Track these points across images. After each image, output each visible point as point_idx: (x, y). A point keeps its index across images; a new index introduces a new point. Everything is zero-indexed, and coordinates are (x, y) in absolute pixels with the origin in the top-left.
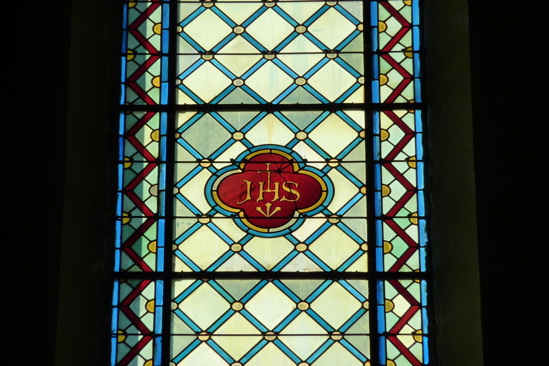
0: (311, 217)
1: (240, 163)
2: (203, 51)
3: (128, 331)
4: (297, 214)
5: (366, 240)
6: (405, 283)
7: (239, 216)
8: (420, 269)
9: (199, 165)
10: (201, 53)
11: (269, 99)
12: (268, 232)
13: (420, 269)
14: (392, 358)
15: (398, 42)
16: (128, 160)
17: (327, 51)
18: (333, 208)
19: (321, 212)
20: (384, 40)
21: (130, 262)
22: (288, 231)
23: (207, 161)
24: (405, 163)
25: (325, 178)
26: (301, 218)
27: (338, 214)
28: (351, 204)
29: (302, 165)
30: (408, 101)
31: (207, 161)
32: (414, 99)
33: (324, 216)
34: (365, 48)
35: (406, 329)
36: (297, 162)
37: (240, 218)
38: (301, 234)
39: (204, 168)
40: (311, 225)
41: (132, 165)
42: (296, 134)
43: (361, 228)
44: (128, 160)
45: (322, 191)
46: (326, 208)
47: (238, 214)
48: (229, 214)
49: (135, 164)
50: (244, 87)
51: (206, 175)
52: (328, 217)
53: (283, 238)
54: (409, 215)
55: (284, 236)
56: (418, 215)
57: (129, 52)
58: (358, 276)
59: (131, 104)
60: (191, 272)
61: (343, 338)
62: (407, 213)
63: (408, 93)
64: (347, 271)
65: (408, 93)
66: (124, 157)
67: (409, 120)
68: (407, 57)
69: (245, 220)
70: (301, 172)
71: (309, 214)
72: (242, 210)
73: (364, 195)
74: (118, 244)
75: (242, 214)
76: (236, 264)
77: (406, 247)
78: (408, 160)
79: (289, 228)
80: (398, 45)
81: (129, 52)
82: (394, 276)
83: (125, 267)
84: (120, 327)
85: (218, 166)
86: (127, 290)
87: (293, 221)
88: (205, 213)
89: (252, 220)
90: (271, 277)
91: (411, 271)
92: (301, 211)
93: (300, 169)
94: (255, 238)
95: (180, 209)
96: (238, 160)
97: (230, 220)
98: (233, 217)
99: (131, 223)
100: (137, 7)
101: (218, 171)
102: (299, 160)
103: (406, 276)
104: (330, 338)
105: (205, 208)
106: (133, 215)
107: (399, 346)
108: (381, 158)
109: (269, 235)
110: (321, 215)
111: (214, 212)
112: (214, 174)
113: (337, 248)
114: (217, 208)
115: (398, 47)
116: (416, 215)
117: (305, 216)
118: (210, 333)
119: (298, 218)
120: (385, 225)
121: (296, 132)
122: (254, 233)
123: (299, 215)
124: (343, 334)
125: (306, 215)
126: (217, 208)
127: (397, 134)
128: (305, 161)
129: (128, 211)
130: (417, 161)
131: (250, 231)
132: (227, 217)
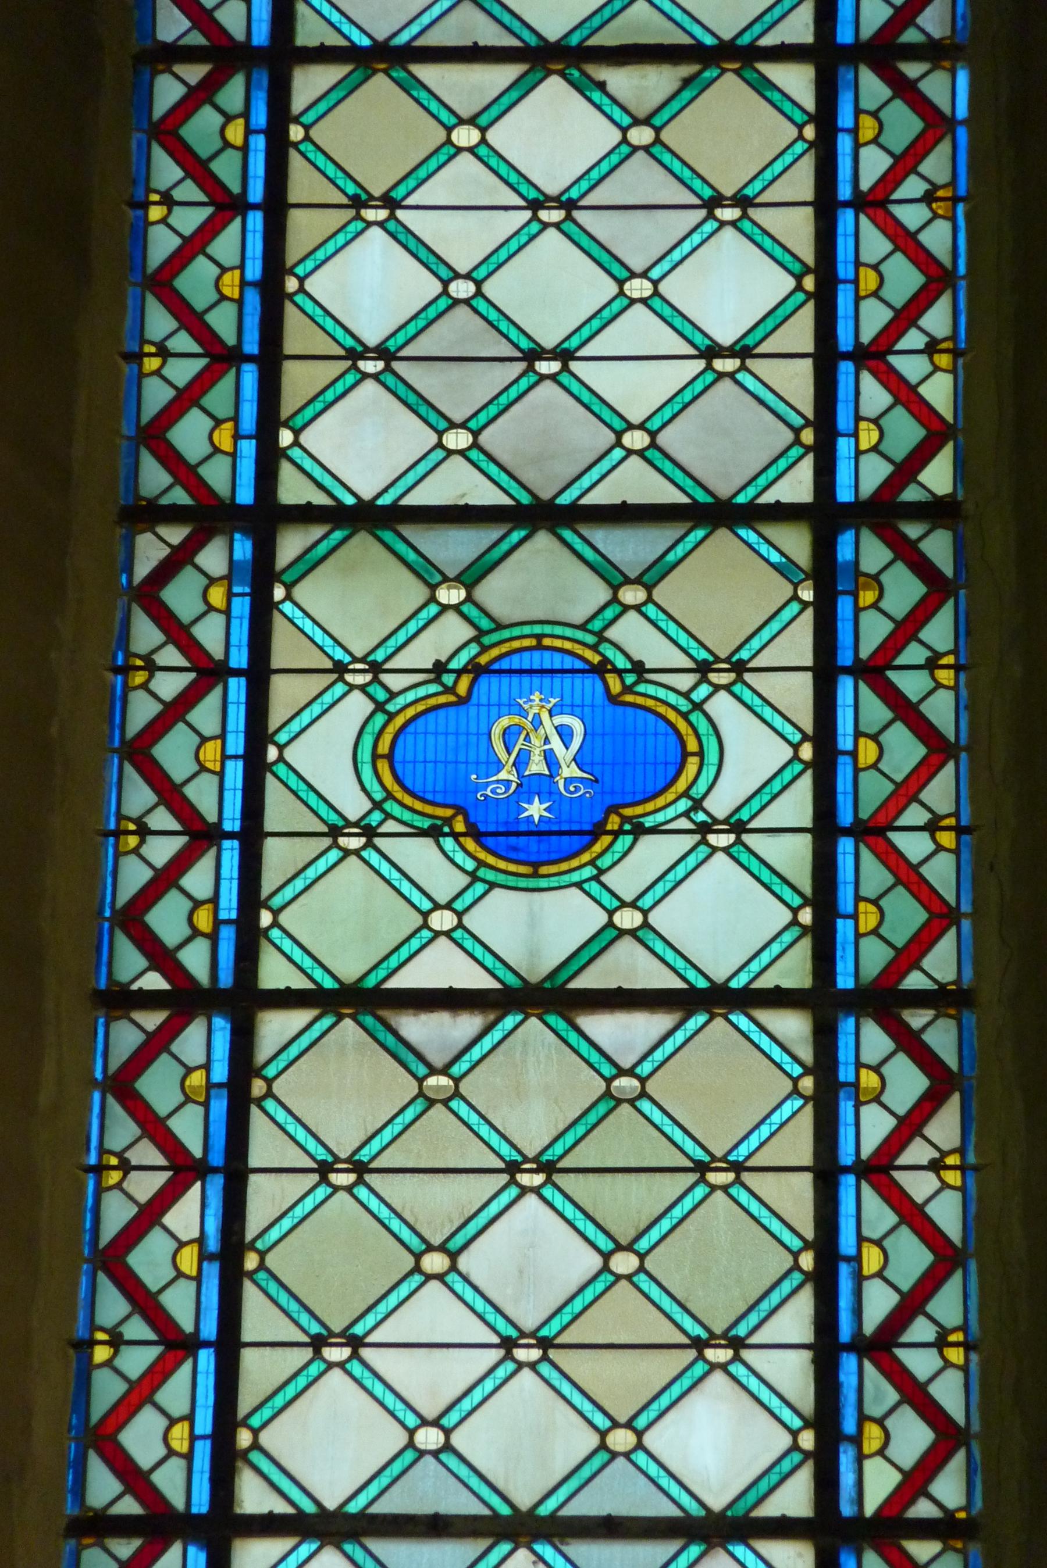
0: (655, 830)
1: (459, 673)
3: (178, 195)
6: (916, 1019)
7: (451, 828)
11: (553, 32)
13: (958, 981)
15: (914, 798)
17: (711, 352)
24: (926, 835)
25: (696, 717)
28: (769, 791)
29: (630, 679)
30: (942, 987)
32: (966, 1508)
34: (817, 1154)
37: (456, 836)
38: (627, 879)
39: (369, 224)
40: (652, 855)
42: (611, 913)
43: (797, 229)
44: (153, 350)
47: (448, 821)
48: (426, 824)
53: (575, 891)
54: (927, 192)
57: (101, 1336)
58: (782, 513)
60: (347, 47)
63: (942, 963)
64: (754, 1514)
65: (942, 963)
66: (102, 1151)
68: (936, 216)
69: (470, 844)
71: (649, 822)
72: (460, 810)
76: (441, 968)
77: (919, 751)
78: (928, 198)
81: (101, 1336)
82: (883, 1000)
89: (490, 841)
90: (535, 1005)
94: (497, 891)
96: (454, 665)
97: (428, 842)
99: (170, 221)
100: (165, 372)
107: (892, 381)
109: (537, 629)
110: (684, 824)
111: (376, 817)
112: (380, 707)
115: (913, 339)
116: (951, 821)
121: (616, 583)
123: (621, 826)
125: (642, 824)
126: (388, 806)
128: (639, 668)
130: (955, 200)
132: (421, 833)
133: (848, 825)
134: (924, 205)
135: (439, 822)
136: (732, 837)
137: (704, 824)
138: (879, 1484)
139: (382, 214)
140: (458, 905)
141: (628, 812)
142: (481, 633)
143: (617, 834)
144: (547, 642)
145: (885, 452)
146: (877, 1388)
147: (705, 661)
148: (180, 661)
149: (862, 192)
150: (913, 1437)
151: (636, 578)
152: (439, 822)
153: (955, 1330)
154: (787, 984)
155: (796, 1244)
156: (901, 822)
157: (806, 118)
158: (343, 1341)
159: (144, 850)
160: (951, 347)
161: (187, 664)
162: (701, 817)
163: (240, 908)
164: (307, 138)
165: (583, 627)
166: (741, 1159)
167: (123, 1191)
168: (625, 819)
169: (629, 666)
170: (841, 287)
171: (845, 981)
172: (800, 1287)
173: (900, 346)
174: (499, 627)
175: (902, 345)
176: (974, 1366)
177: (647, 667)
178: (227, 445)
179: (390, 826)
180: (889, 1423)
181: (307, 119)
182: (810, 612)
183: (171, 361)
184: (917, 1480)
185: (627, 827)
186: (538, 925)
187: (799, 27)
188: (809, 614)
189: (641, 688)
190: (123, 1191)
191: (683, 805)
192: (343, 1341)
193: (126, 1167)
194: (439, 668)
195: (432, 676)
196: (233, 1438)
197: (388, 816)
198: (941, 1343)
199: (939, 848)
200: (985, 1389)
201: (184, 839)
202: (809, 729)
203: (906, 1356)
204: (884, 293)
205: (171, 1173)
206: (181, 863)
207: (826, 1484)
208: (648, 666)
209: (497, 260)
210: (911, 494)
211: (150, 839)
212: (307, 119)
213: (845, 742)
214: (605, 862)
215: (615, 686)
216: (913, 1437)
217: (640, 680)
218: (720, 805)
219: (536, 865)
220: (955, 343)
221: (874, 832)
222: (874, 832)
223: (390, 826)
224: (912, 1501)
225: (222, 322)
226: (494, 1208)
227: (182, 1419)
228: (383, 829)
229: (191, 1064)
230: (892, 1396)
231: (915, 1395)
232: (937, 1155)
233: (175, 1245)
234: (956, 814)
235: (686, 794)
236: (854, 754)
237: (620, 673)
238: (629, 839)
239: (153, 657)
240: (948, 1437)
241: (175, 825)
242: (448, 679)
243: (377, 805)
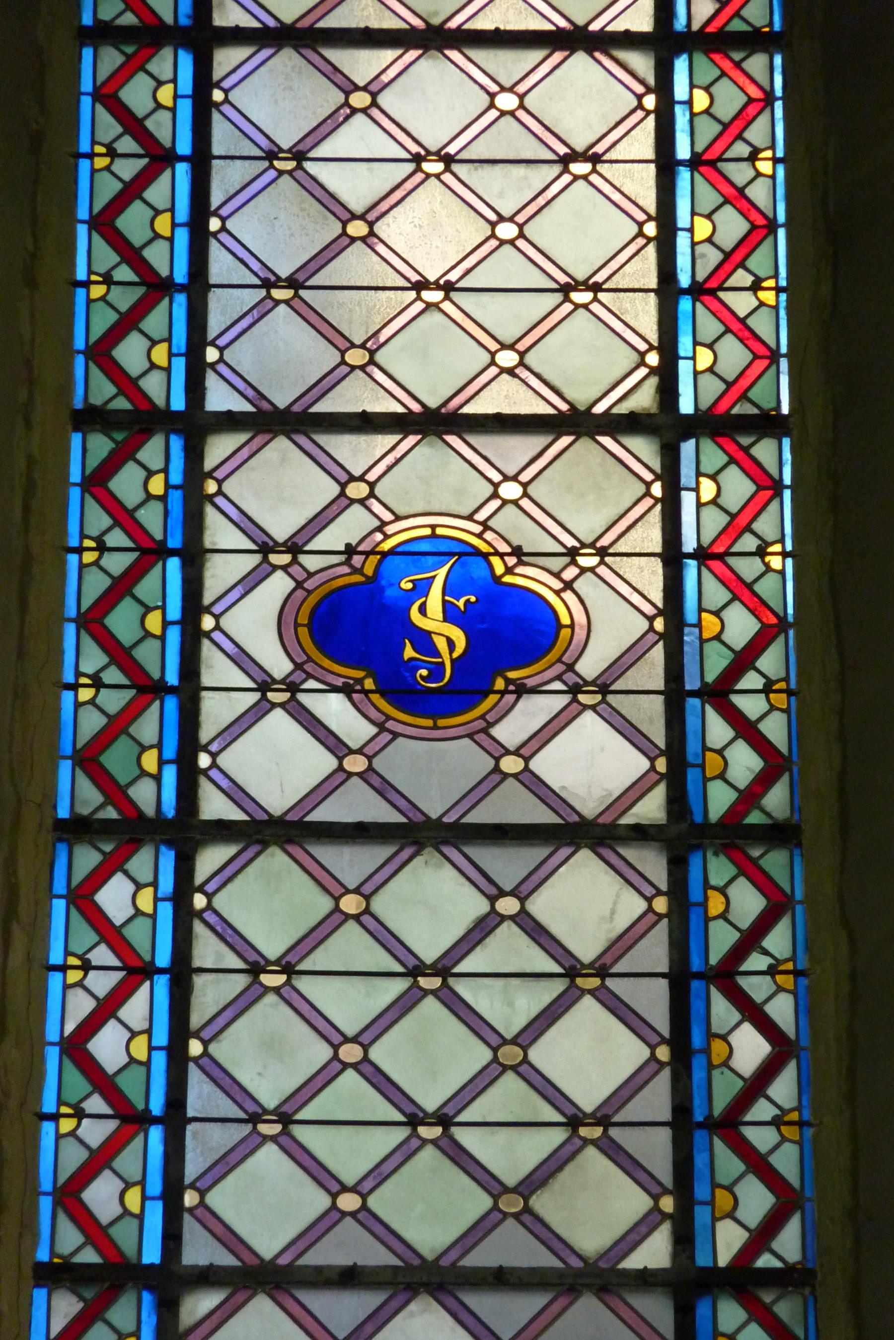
0: (535, 691)
1: (367, 554)
2: (273, 278)
4: (500, 684)
5: (656, 344)
7: (362, 685)
8: (771, 24)
9: (272, 166)
10: (267, 285)
12: (435, 727)
14: (718, 746)
16: (103, 150)
18: (589, 666)
19: (559, 678)
20: (722, 940)
21: (110, 389)
22: (481, 724)
23: (289, 155)
25: (568, 596)
26: (511, 692)
27: (598, 545)
31: (289, 155)
33: (564, 688)
35: (762, 1110)
36: (497, 553)
38: (511, 731)
41: (100, 558)
44: (103, 150)
45: (559, 626)
46: (570, 667)
47: (360, 681)
48: (339, 682)
49: (92, 974)
50: (365, 1217)
51: (278, 586)
52: (574, 690)
53: (467, 741)
54: (770, 966)
55: (470, 736)
56: (795, 965)
59: (66, 1259)
61: (602, 562)
62: (773, 1112)
65: (789, 1243)
67: (775, 862)
68: (784, 1139)
70: (508, 579)
71: (530, 683)
73: (657, 500)
74: (75, 475)
75: (369, 684)
76: (357, 805)
78: (776, 1122)
79: (483, 717)
80: (740, 272)
83: (97, 400)
84: (72, 948)
85: (311, 562)
86: (101, 446)
87: (493, 698)
88: (284, 276)
91: (750, 29)
92: (512, 675)
93: (509, 571)
94: (400, 740)
95: (217, 669)
98: (347, 690)
101: (310, 575)
102: (504, 548)
103: (770, 1277)
104: (575, 700)
105: (278, 665)
106: (116, 279)
108: (710, 1116)
110: (558, 686)
112: (299, 585)
113: (593, 763)
114: (308, 667)
115: (751, 681)
117: (521, 690)
118: (285, 1118)
119: (503, 693)
120: (710, 711)
122: (400, 728)
124: (603, 553)
125: (524, 685)
127: (748, 902)
129: (74, 1101)
131: (390, 725)
132: (334, 689)
133: (692, 551)
134: (751, 292)
135: (352, 682)
136: (599, 697)
137: (576, 685)
138: (729, 1241)
139: (276, 1129)
140: (369, 750)
141: (512, 675)
142: (485, 731)
143: (503, 693)
144: (439, 531)
145: (722, 513)
146: (729, 1245)
147: (574, 547)
148: (111, 960)
149: (698, 282)
150: (756, 1200)
151: (512, 1039)
152: (352, 682)
153: (787, 960)
154: (634, 28)
155: (649, 610)
156: (729, 283)
157: (658, 752)
158: (284, 687)
159: (103, 562)
160: (785, 687)
161: (127, 682)
162: (570, 678)
163: (184, 609)
164: (217, 627)
165: (470, 518)
166: (600, 281)
167: (102, 569)
168: (508, 681)
169: (509, 550)
170: (680, 233)
171: (686, 406)
172: (656, 643)
173: (741, 686)
174: (398, 518)
175: (742, 685)
176: (801, 989)
177: (525, 551)
178: (135, 1208)
179: (311, 684)
180: (737, 1190)
181: (217, 609)
182: (652, 117)
183: (103, 691)
184: (763, 1236)
185: (512, 688)
186: (435, 769)
187: (641, 20)
188: (651, 120)
189: (519, 570)
190: (102, 569)
191: (559, 668)
192: (284, 687)
193: (86, 967)
194: (350, 551)
195: (342, 558)
196: (198, 622)
197: (557, 575)
198: (767, 689)
199: (772, 708)
200: (814, 1158)
201: (121, 974)
202: (652, 211)
203: (750, 1133)
204: (740, 1214)
205: (125, 973)
206: (134, 574)
207: (684, 1240)
208: (526, 550)
209: (380, 1174)
210: (754, 818)
211: (85, 1121)
212: (217, 609)
213: (691, 615)
214: (300, 594)
215: (499, 569)
216: (756, 1200)
217: (520, 563)
218: (589, 666)
219: (434, 536)
220: (788, 684)
221: (719, 694)
222: (719, 694)
223: (555, 564)
224: (746, 814)
225: (151, 519)
226: (409, 185)
227: (135, 1184)
228: (305, 686)
229: (146, 744)
230: (739, 1166)
231: (759, 1165)
232: (778, 1112)
233: (128, 1035)
234: (793, 958)
235: (559, 660)
236: (690, 103)
237: (502, 555)
238: (512, 697)
239: (102, 675)
240: (787, 1202)
241: (114, 962)
242: (357, 560)
243: (298, 666)
